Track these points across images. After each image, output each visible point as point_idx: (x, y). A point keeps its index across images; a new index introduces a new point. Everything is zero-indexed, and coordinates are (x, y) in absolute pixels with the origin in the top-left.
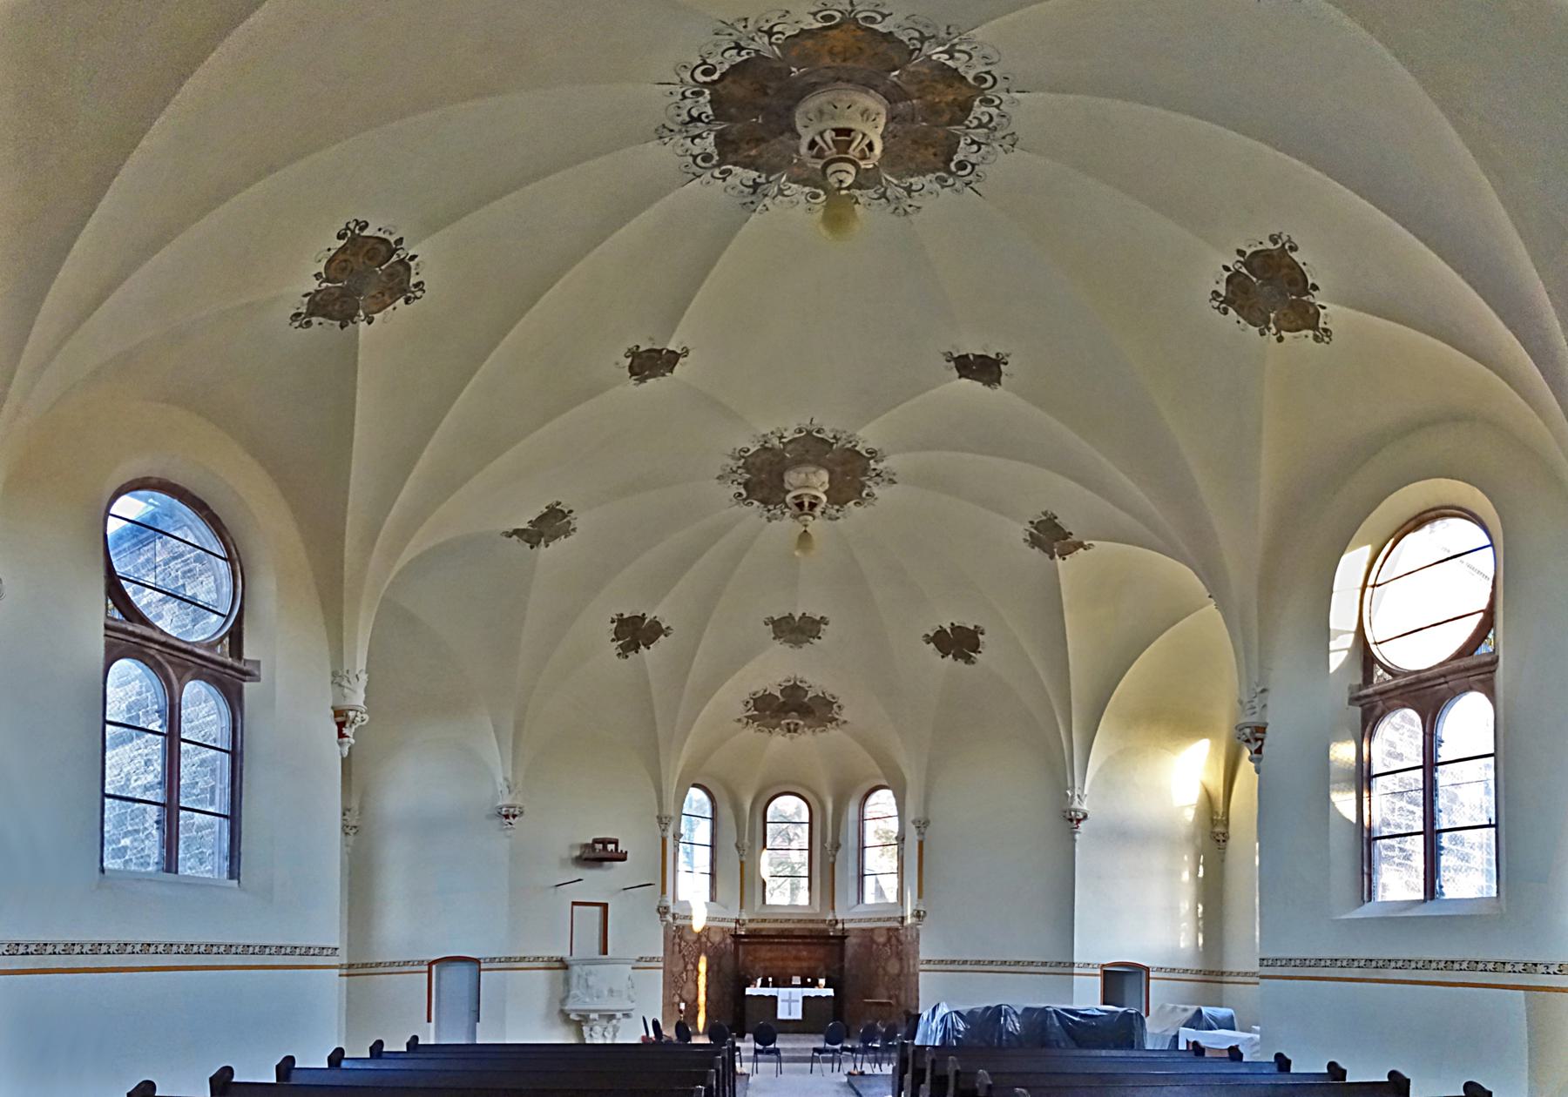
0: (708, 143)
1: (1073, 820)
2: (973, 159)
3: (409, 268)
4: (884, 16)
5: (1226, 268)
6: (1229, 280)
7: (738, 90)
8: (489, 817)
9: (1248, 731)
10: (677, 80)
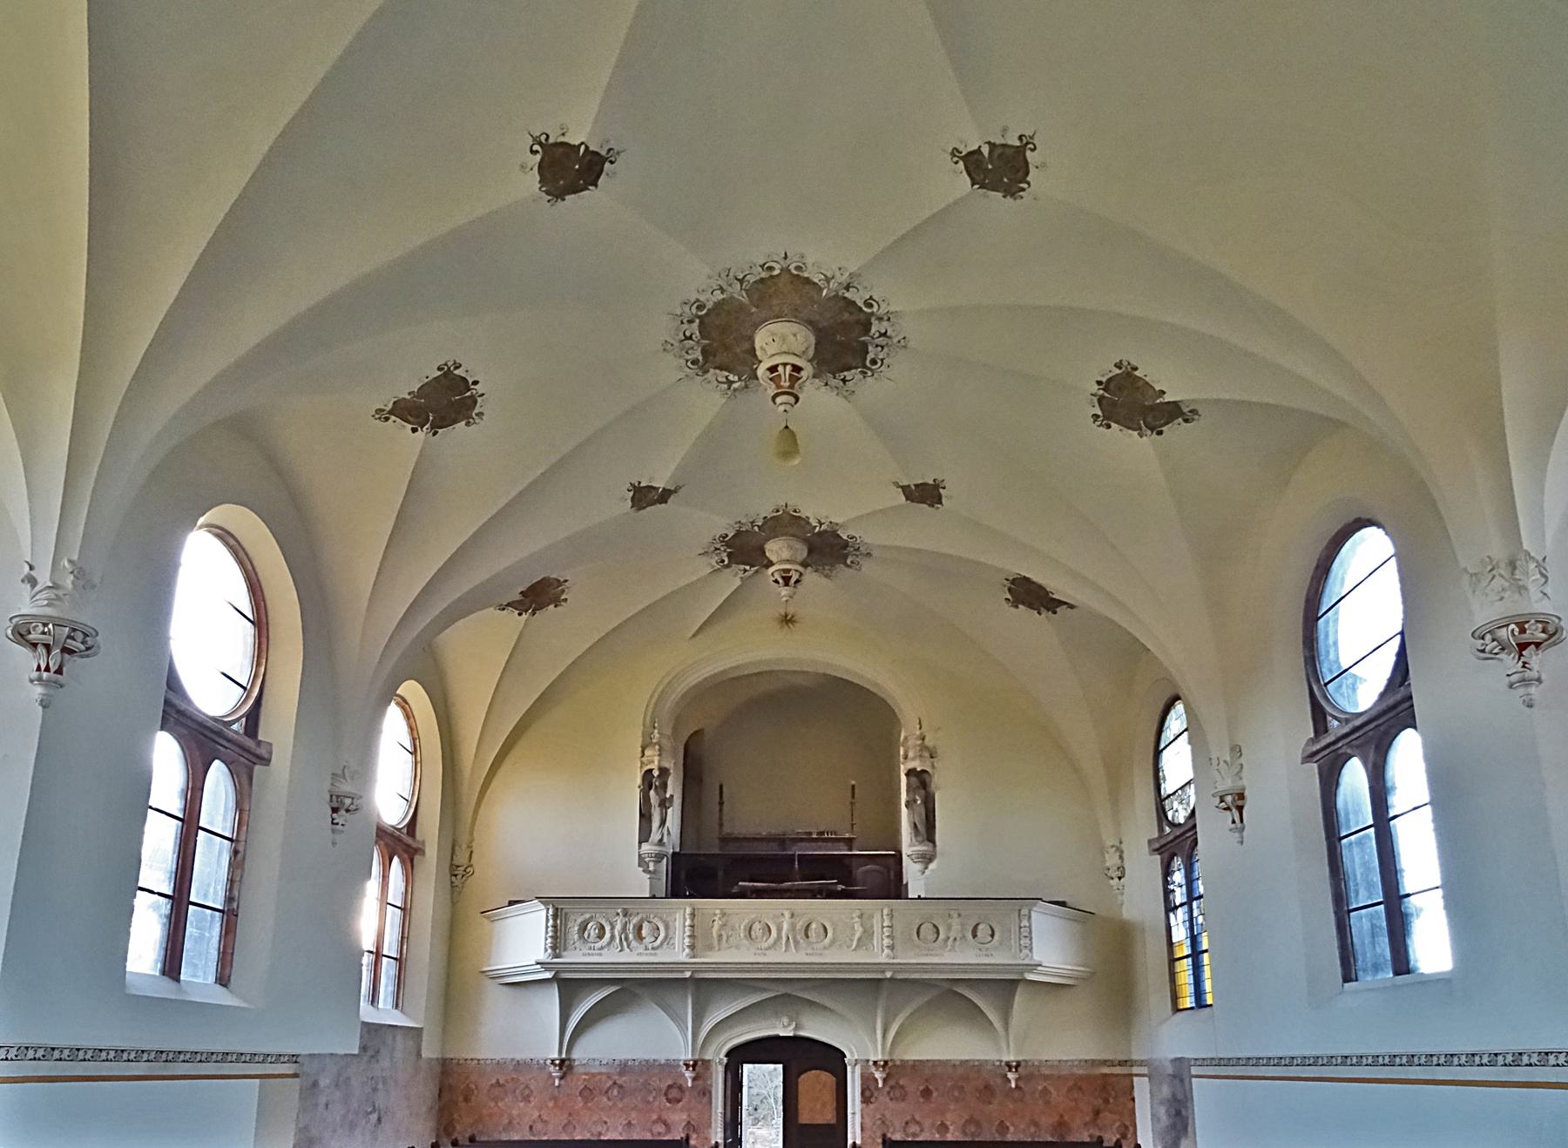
1: (414, 753)
2: (685, 326)
3: (1110, 380)
5: (476, 383)
6: (464, 379)
7: (849, 359)
9: (1229, 799)
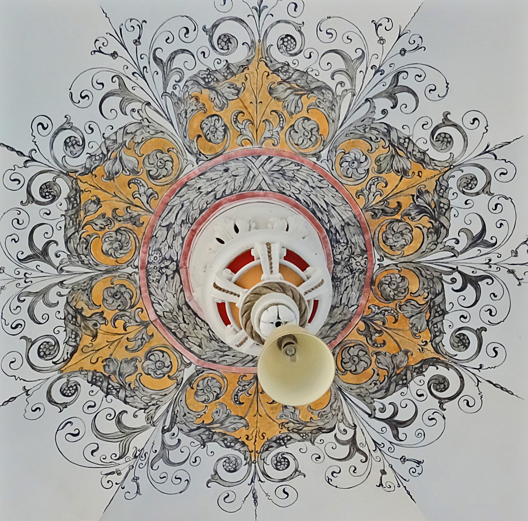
0: (461, 219)
4: (215, 477)
8: (262, 243)
10: (484, 385)
